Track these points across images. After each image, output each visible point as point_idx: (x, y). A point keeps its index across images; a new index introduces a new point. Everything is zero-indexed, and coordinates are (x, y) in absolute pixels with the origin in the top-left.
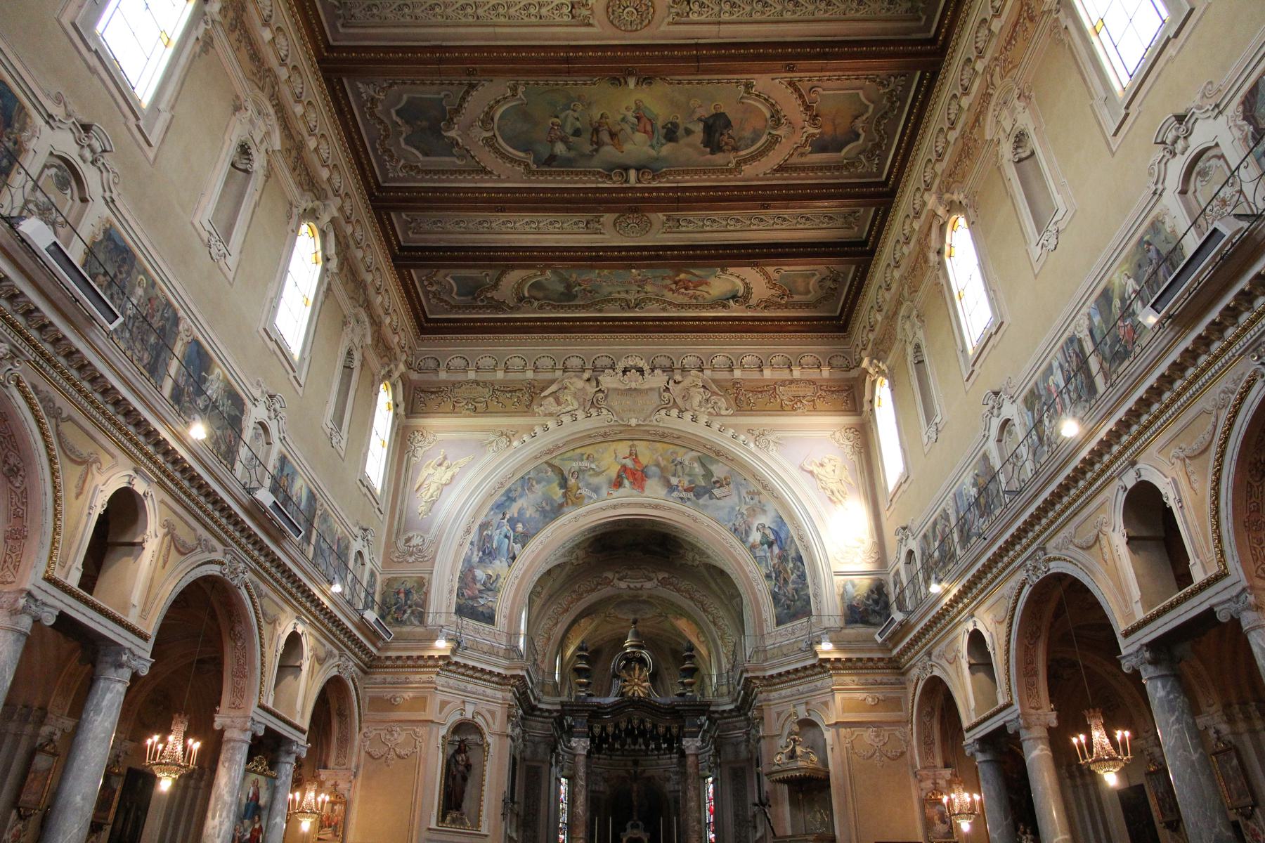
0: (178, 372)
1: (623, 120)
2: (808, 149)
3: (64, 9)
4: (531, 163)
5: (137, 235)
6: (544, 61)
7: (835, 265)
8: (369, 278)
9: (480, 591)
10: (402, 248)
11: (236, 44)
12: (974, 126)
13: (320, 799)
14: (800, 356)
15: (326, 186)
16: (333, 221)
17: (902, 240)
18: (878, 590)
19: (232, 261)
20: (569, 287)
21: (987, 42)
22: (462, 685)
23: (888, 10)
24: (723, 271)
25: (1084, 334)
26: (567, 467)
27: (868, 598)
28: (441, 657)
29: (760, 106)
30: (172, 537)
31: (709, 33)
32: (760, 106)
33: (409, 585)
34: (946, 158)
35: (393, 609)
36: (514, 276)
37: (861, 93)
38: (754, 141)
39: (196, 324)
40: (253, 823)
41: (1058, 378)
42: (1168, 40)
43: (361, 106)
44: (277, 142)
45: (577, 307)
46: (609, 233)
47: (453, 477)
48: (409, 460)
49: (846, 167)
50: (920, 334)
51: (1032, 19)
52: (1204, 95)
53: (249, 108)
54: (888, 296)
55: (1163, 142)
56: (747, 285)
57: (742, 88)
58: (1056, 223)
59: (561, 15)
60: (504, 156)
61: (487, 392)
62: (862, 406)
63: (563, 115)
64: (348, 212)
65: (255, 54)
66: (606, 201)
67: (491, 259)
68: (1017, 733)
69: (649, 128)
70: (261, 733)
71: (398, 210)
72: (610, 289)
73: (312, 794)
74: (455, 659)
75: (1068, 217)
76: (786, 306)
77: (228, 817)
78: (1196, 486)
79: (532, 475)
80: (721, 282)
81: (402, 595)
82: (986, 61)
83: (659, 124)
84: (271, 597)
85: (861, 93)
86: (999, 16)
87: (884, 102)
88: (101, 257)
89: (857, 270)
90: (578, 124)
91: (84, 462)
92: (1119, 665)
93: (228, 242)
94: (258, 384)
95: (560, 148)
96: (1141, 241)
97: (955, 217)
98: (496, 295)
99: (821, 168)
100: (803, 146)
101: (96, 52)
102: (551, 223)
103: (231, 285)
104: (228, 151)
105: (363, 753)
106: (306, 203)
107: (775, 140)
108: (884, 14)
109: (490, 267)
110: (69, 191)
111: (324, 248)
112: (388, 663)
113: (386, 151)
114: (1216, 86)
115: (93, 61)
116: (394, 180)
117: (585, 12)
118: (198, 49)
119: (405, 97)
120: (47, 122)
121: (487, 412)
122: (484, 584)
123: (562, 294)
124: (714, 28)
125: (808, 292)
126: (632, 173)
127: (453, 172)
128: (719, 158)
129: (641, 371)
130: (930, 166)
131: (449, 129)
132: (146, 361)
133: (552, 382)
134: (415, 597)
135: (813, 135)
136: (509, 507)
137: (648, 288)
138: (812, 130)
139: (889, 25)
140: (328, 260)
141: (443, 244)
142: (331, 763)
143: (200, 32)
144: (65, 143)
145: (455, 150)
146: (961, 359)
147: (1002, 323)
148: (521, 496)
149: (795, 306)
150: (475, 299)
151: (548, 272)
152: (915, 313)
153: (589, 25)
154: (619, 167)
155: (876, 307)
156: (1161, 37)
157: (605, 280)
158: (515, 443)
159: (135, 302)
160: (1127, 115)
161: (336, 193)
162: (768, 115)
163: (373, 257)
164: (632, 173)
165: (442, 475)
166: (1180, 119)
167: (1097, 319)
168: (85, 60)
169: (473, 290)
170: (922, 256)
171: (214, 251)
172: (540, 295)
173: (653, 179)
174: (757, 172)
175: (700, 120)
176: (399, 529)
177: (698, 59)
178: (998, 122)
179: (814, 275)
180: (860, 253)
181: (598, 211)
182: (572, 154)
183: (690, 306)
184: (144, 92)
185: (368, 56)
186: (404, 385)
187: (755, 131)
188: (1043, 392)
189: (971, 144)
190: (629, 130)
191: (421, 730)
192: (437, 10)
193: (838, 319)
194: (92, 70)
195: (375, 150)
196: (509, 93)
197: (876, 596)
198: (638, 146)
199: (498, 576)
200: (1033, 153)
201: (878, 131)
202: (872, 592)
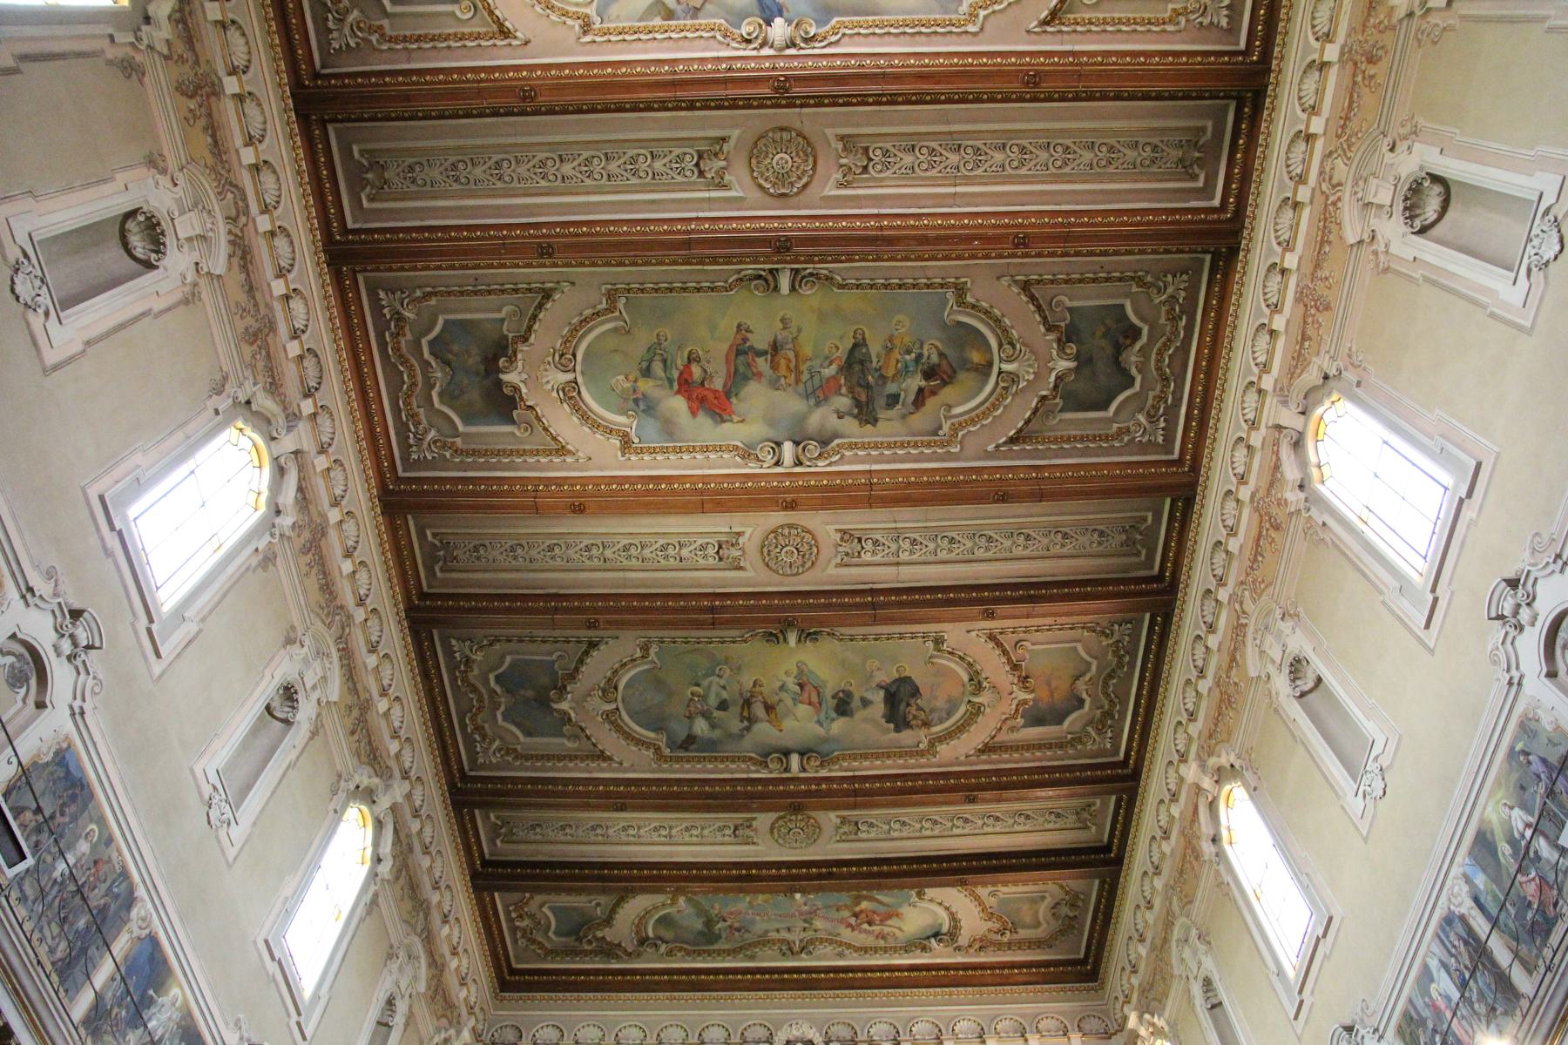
0: (105, 986)
1: (782, 688)
2: (1020, 721)
4: (663, 746)
5: (106, 768)
6: (684, 610)
7: (1073, 881)
8: (435, 898)
10: (485, 863)
11: (305, 569)
12: (1230, 668)
14: (1036, 1018)
15: (392, 763)
16: (394, 808)
17: (1159, 834)
19: (237, 833)
20: (709, 923)
21: (1227, 567)
23: (1100, 543)
24: (920, 895)
25: (1466, 907)
29: (953, 666)
31: (885, 576)
32: (953, 666)
34: (1252, 480)
37: (1079, 646)
38: (949, 714)
39: (159, 911)
41: (1444, 985)
42: (1461, 501)
43: (452, 669)
44: (335, 690)
45: (719, 952)
46: (765, 842)
49: (1072, 743)
50: (1208, 964)
51: (1277, 528)
53: (307, 643)
54: (1150, 917)
55: (1501, 617)
56: (953, 918)
57: (930, 644)
58: (1376, 758)
59: (705, 557)
63: (705, 683)
64: (418, 803)
65: (327, 585)
66: (762, 796)
67: (602, 878)
69: (815, 698)
71: (484, 805)
72: (765, 926)
75: (1391, 747)
76: (1009, 945)
80: (922, 911)
82: (1230, 588)
83: (828, 692)
85: (1079, 646)
86: (1235, 535)
87: (1110, 657)
88: (39, 786)
89: (1102, 883)
90: (725, 695)
93: (238, 808)
94: (237, 1023)
95: (701, 727)
96: (1511, 754)
97: (1227, 788)
98: (608, 934)
99: (1039, 747)
100: (1014, 717)
101: (120, 533)
102: (687, 829)
103: (229, 866)
104: (266, 690)
106: (365, 778)
107: (976, 711)
108: (1095, 548)
109: (604, 891)
110: (23, 691)
111: (376, 843)
114: (1546, 537)
115: (113, 542)
116: (483, 767)
117: (735, 553)
118: (254, 561)
119: (508, 659)
120: (23, 597)
123: (701, 933)
124: (893, 569)
125: (1038, 924)
126: (795, 760)
127: (561, 758)
128: (907, 737)
130: (1180, 730)
131: (561, 699)
132: (59, 955)
135: (1025, 702)
137: (818, 924)
138: (1023, 696)
139: (1101, 561)
140: (379, 860)
143: (262, 544)
145: (566, 729)
146: (1279, 987)
147: (1330, 919)
150: (579, 939)
151: (682, 900)
152: (1194, 932)
153: (741, 568)
154: (776, 751)
155: (1136, 936)
156: (1450, 504)
157: (760, 912)
159: (71, 861)
160: (1436, 600)
161: (405, 775)
162: (966, 678)
163: (445, 867)
164: (795, 760)
166: (1513, 583)
167: (1480, 880)
168: (102, 540)
170: (1191, 850)
171: (214, 814)
172: (668, 935)
173: (822, 765)
174: (957, 753)
175: (880, 686)
177: (874, 606)
178: (1262, 652)
179: (1043, 898)
180: (1104, 860)
181: (750, 810)
182: (717, 734)
183: (876, 950)
184: (167, 598)
185: (467, 605)
187: (949, 701)
188: (1426, 1013)
189: (1231, 690)
190: (789, 702)
192: (557, 550)
193: (1083, 962)
194: (108, 553)
195: (463, 727)
196: (638, 654)
198: (801, 723)
200: (1319, 680)
201: (1106, 694)
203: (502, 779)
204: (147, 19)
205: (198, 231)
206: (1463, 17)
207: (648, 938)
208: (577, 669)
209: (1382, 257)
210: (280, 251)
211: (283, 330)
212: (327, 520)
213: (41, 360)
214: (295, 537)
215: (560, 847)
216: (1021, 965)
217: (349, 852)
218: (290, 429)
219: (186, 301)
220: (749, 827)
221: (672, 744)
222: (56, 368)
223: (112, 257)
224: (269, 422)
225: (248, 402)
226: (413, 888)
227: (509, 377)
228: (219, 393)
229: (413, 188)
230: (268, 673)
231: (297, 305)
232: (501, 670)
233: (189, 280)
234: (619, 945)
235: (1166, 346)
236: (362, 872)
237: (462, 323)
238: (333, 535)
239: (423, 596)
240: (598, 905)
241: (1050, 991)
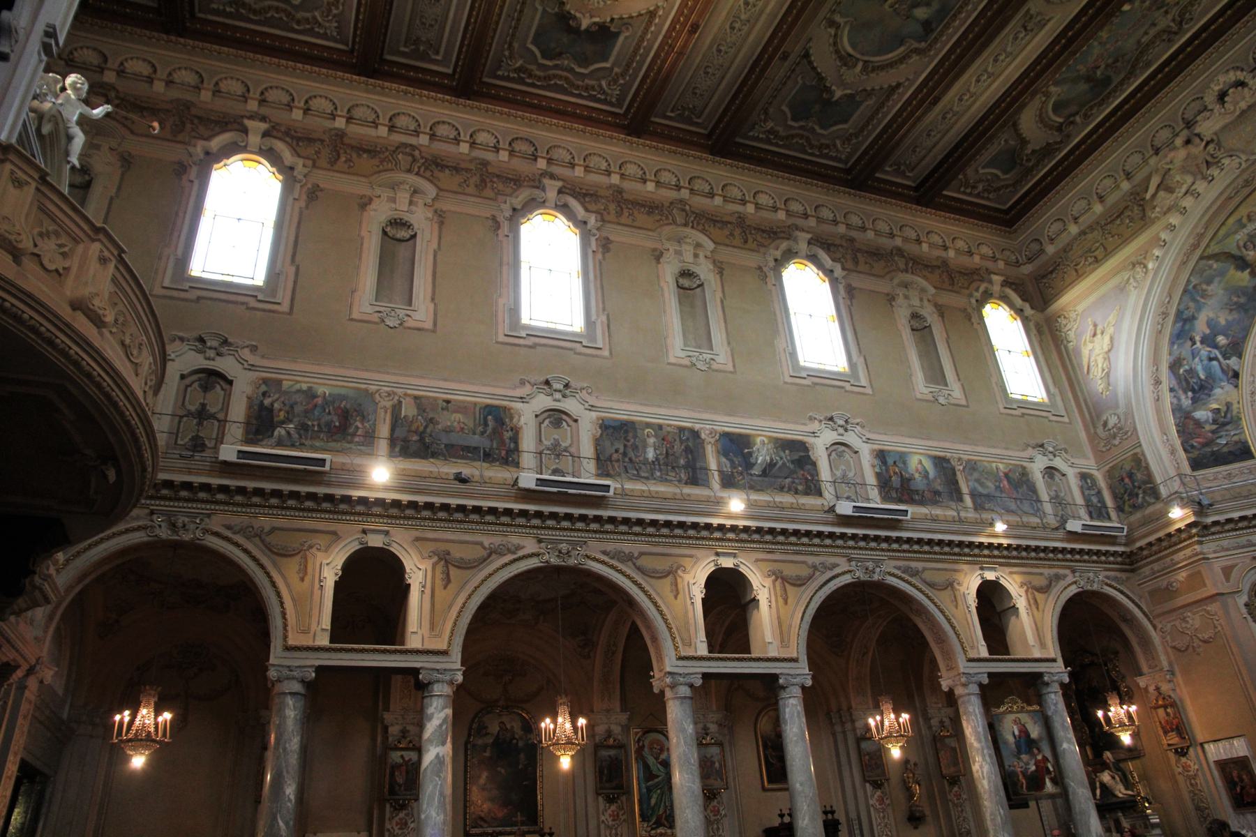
3: (497, 333)
4: (916, 45)
9: (1213, 432)
10: (916, 189)
20: (1089, 79)
22: (1243, 540)
26: (1231, 245)
28: (1189, 526)
30: (783, 579)
33: (1127, 467)
35: (1126, 497)
36: (1028, 121)
40: (1033, 756)
43: (768, 142)
45: (1121, 83)
47: (1112, 339)
48: (1066, 348)
60: (892, 65)
61: (1096, 234)
68: (662, 692)
70: (986, 681)
74: (1209, 520)
77: (984, 760)
79: (1194, 281)
81: (1127, 480)
84: (932, 569)
91: (671, 573)
105: (1169, 650)
112: (1145, 553)
113: (820, 147)
118: (600, 256)
119: (784, 108)
121: (1108, 254)
122: (1215, 421)
129: (1241, 84)
133: (1148, 178)
134: (1139, 476)
136: (1192, 329)
140: (832, 271)
141: (940, 158)
142: (1145, 669)
144: (543, 401)
145: (858, 98)
148: (1199, 309)
151: (1053, 89)
158: (1150, 266)
165: (1102, 343)
168: (525, 346)
169: (1011, 159)
172: (1074, 108)
176: (1091, 417)
186: (1015, 290)
191: (1213, 607)
196: (832, 31)
199: (1228, 405)
203: (865, 152)
204: (292, 168)
205: (408, 196)
207: (1061, 124)
208: (818, 74)
210: (445, 134)
211: (490, 156)
212: (615, 185)
213: (426, 330)
214: (608, 217)
215: (941, 144)
217: (807, 292)
218: (544, 190)
219: (441, 224)
220: (1031, 18)
221: (920, 39)
222: (435, 324)
223: (403, 250)
224: (533, 199)
225: (514, 209)
226: (875, 254)
227: (585, 24)
228: (499, 227)
229: (436, 27)
230: (662, 284)
231: (482, 138)
232: (789, 115)
233: (430, 215)
234: (1048, 144)
236: (826, 287)
237: (537, 34)
238: (627, 185)
239: (709, 136)
240: (1006, 141)
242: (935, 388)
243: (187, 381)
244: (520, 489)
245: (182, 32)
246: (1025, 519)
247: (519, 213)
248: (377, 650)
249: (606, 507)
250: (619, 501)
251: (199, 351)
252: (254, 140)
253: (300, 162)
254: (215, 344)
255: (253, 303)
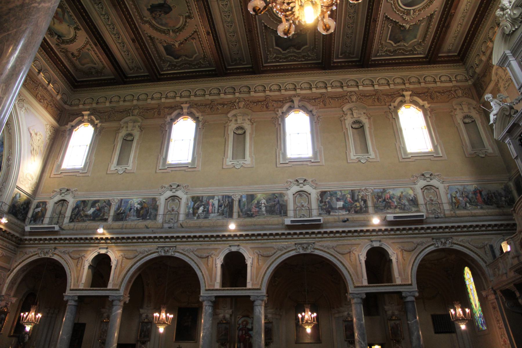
13: (37, 316)
18: (27, 203)
25: (236, 199)
27: (22, 205)
52: (312, 181)
57: (187, 14)
62: (67, 124)
73: (33, 314)
78: (260, 263)
92: (199, 298)
128: (146, 13)
149: (71, 62)
197: (25, 206)
202: (25, 203)
206: (392, 123)
209: (343, 118)
216: (64, 65)
235: (295, 57)
241: (63, 78)
242: (360, 156)
243: (295, 195)
244: (387, 221)
245: (159, 80)
246: (505, 210)
247: (285, 114)
248: (374, 286)
249: (322, 228)
250: (428, 220)
251: (424, 180)
252: (185, 111)
253: (426, 102)
254: (302, 182)
255: (78, 174)
